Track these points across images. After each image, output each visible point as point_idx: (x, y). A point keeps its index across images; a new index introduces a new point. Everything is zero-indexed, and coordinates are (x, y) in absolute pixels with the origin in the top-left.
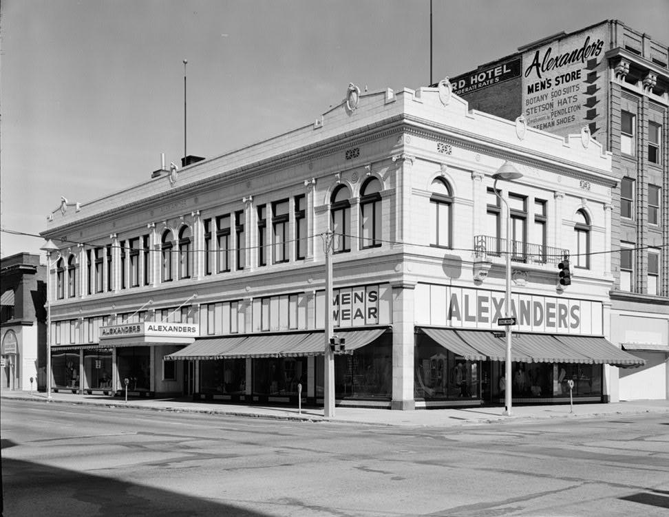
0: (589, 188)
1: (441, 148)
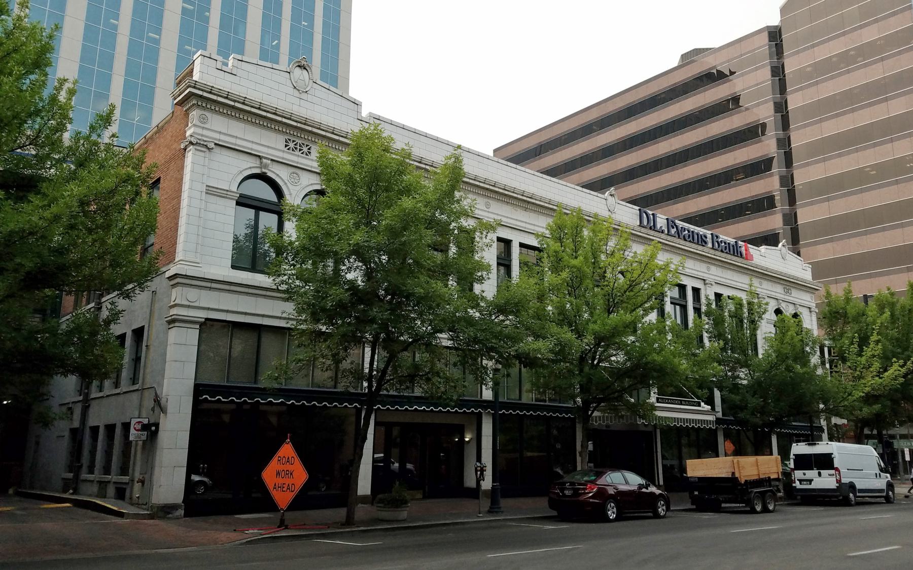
0: (791, 294)
1: (292, 145)
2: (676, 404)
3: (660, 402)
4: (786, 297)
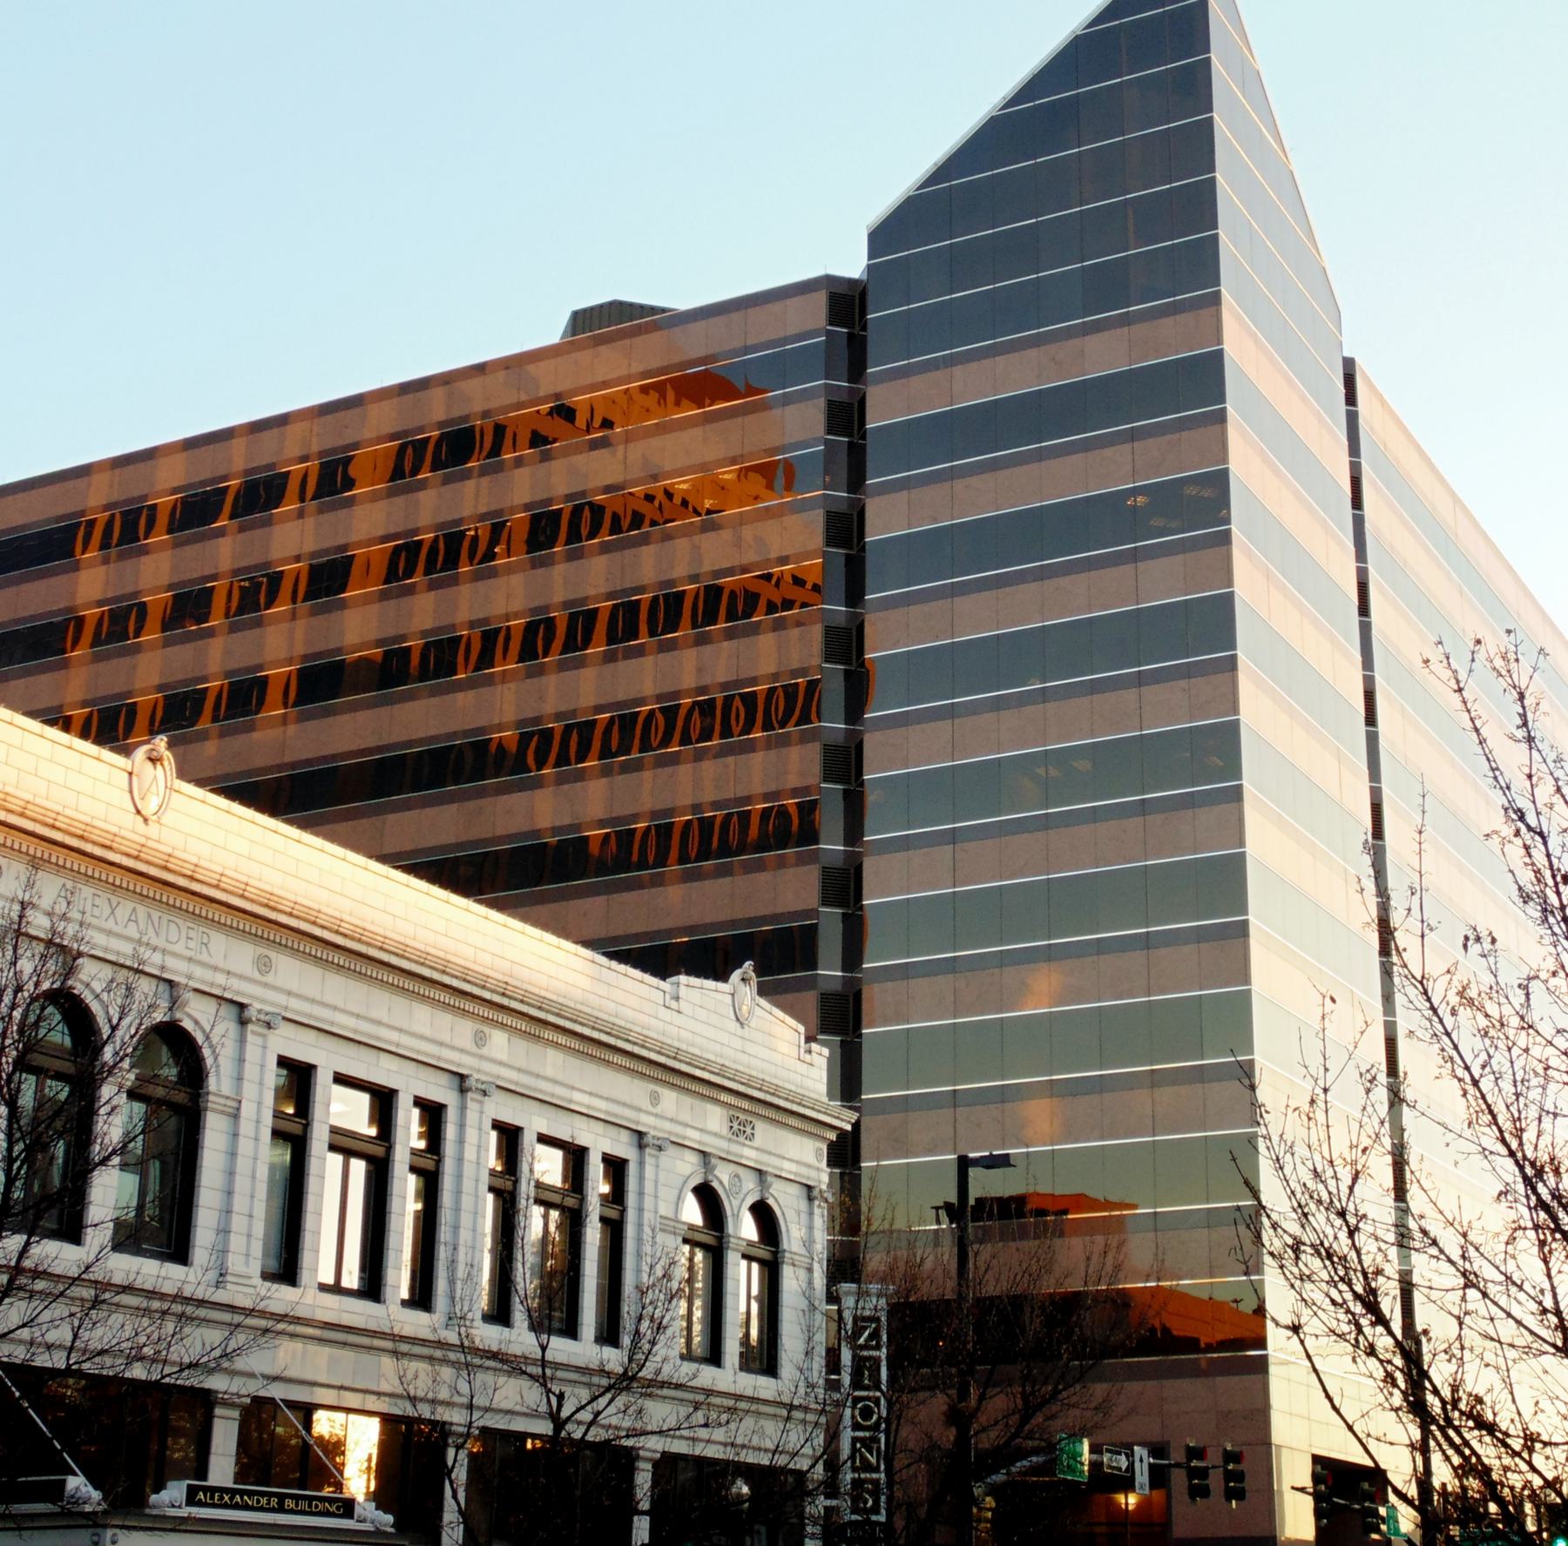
2: (261, 1509)
3: (201, 1504)
4: (735, 1148)
